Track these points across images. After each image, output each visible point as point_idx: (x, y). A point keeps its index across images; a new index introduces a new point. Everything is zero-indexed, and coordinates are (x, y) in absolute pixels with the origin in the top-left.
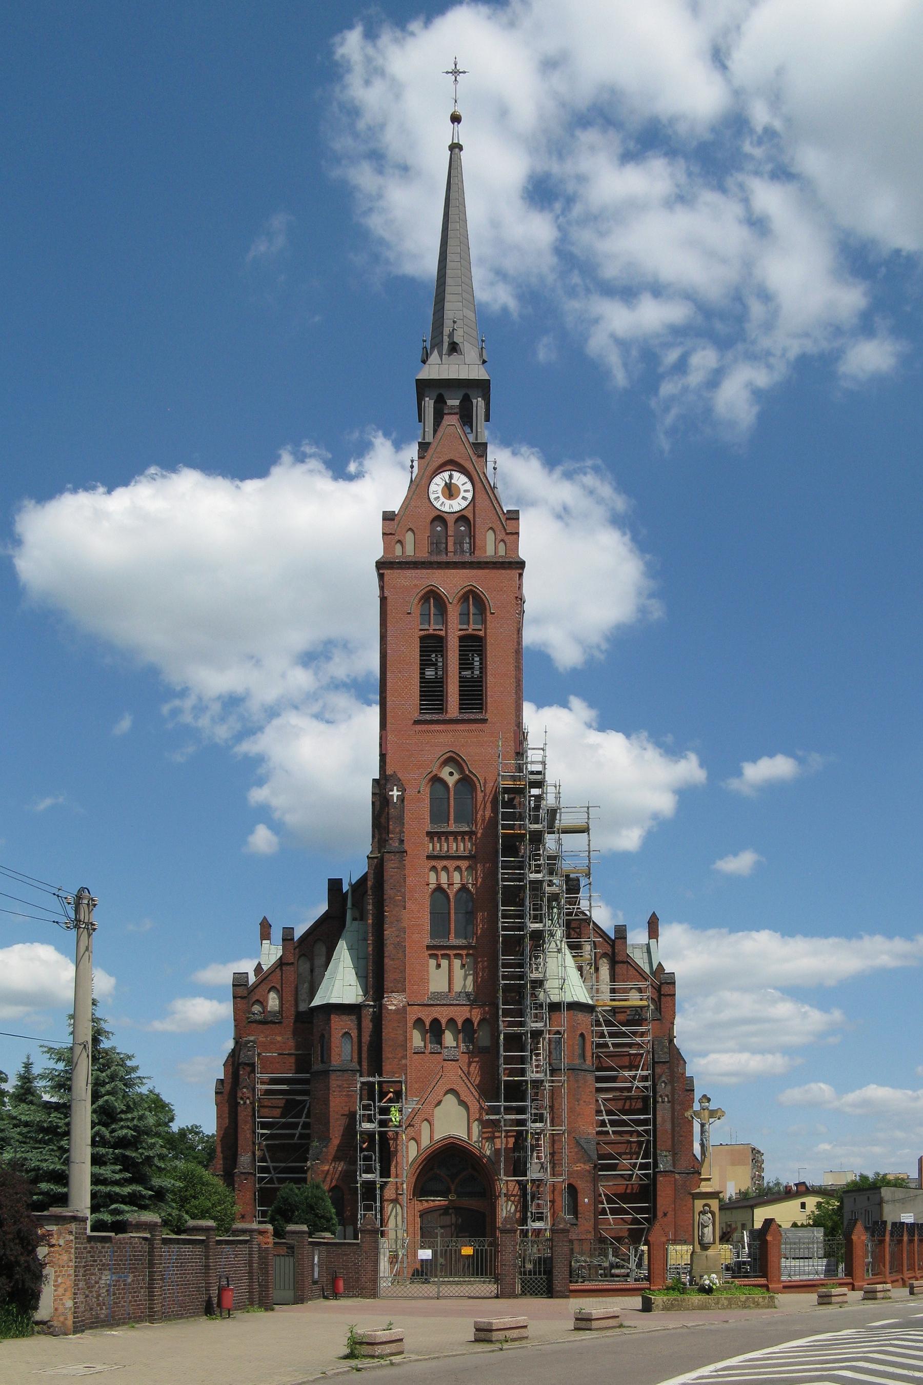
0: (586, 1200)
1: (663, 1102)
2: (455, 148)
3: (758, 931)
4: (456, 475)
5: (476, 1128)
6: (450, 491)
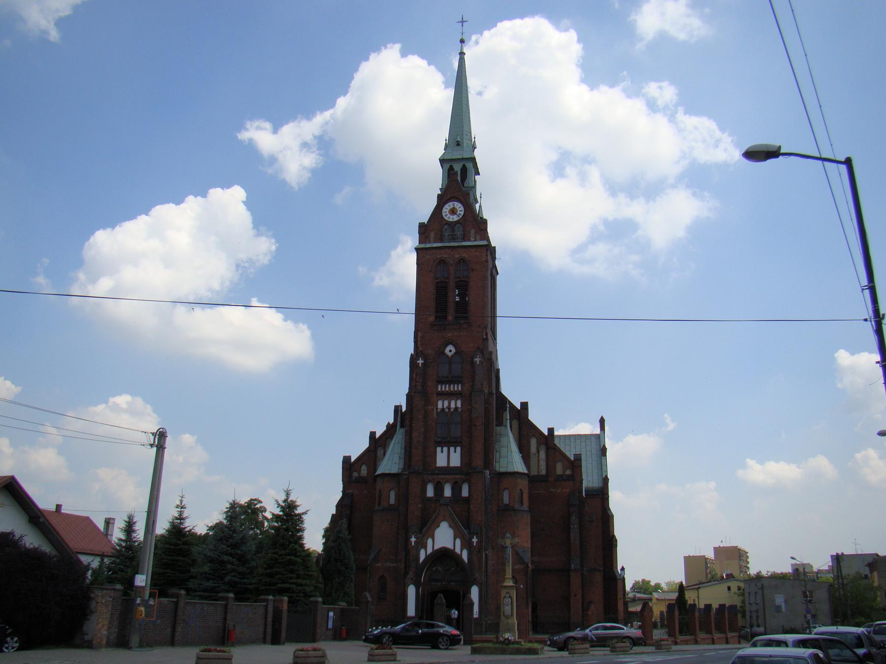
4: (456, 203)
5: (458, 542)
6: (453, 211)
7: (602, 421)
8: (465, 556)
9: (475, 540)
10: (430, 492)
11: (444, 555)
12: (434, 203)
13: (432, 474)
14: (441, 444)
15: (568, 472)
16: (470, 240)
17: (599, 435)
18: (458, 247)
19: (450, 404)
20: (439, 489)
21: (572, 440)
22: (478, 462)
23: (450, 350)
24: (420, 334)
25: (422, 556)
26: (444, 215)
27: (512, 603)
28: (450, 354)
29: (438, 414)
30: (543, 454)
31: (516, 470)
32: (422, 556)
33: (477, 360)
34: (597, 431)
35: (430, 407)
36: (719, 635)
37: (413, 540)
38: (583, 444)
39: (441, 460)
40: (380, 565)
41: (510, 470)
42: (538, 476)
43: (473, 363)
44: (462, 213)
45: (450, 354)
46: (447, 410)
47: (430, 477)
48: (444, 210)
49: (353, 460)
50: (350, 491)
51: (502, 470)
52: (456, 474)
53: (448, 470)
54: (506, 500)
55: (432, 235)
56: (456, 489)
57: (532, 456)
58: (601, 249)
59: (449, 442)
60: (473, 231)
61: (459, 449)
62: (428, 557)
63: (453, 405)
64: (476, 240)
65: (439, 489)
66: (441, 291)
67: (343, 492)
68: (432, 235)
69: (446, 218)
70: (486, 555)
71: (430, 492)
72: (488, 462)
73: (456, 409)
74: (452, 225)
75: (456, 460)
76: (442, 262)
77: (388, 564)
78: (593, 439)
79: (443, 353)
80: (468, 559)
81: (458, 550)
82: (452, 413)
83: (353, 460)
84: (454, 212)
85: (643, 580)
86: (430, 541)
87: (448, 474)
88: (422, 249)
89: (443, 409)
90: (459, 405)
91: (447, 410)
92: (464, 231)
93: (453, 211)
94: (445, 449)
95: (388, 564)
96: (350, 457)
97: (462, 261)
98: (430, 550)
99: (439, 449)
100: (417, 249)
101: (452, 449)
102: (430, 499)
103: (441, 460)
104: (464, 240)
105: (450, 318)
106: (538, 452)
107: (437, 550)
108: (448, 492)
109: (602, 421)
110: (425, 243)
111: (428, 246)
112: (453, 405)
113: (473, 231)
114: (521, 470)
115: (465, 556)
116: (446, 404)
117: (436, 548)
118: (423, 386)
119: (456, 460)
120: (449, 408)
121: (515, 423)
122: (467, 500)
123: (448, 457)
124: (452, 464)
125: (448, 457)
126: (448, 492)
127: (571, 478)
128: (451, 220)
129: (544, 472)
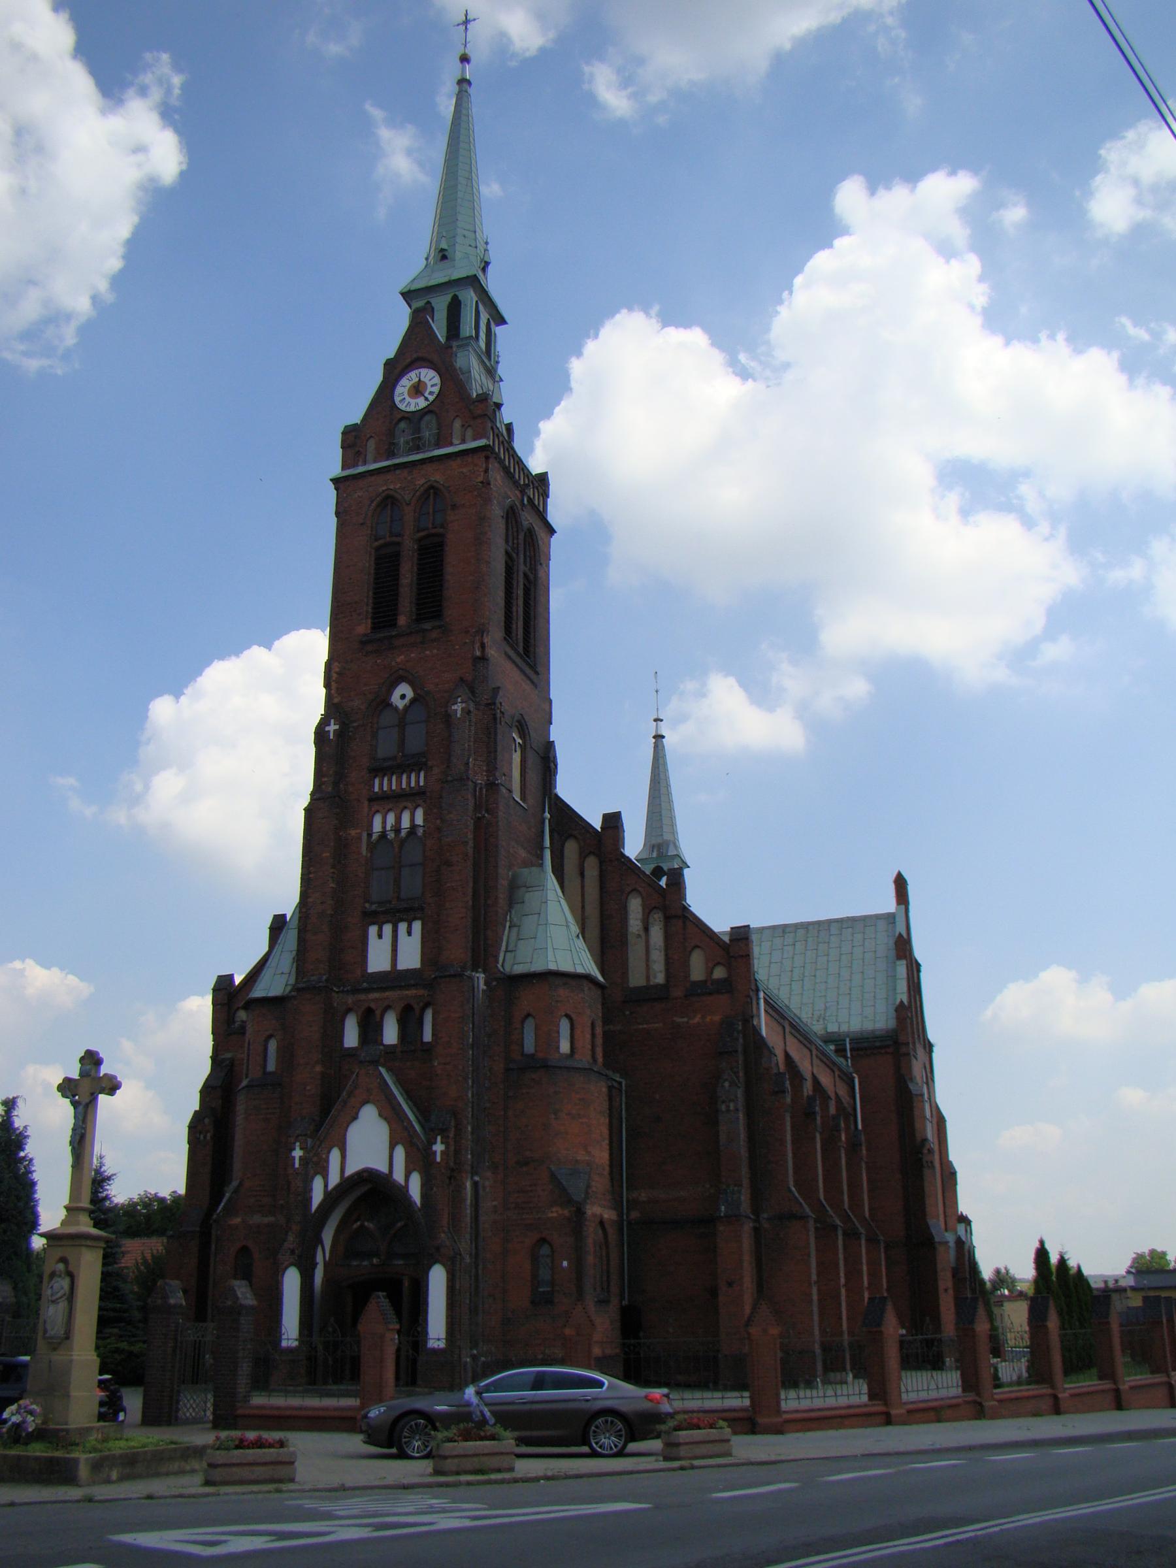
0: (565, 1263)
1: (728, 1110)
2: (463, 82)
3: (380, 1115)
4: (424, 371)
5: (400, 1153)
6: (417, 390)
7: (900, 884)
8: (415, 1190)
9: (439, 1147)
10: (351, 1037)
11: (370, 1189)
12: (378, 377)
13: (356, 991)
14: (376, 917)
15: (719, 973)
16: (451, 444)
17: (890, 918)
18: (423, 461)
19: (398, 820)
20: (370, 1028)
21: (834, 930)
22: (457, 951)
23: (401, 695)
24: (336, 667)
25: (317, 1197)
26: (397, 399)
27: (71, 1297)
28: (400, 704)
29: (372, 847)
30: (657, 934)
31: (552, 967)
32: (317, 1197)
33: (458, 708)
34: (888, 904)
35: (353, 832)
36: (1141, 1377)
37: (298, 1153)
38: (859, 937)
39: (378, 959)
40: (238, 1220)
41: (538, 966)
42: (647, 988)
43: (448, 718)
44: (436, 390)
45: (400, 704)
46: (391, 835)
47: (350, 1000)
48: (399, 390)
49: (238, 980)
50: (229, 1055)
51: (519, 969)
52: (408, 987)
53: (394, 979)
54: (529, 1046)
55: (371, 445)
56: (409, 1021)
57: (631, 939)
58: (1058, 651)
59: (395, 912)
60: (457, 424)
61: (417, 926)
62: (333, 1198)
63: (406, 823)
64: (463, 441)
65: (370, 1028)
66: (386, 564)
67: (215, 1059)
68: (371, 445)
69: (402, 407)
70: (475, 1184)
71: (351, 1037)
72: (483, 950)
73: (413, 827)
74: (408, 417)
75: (411, 956)
76: (389, 501)
77: (257, 1219)
78: (882, 925)
79: (386, 704)
80: (424, 1196)
81: (399, 1176)
82: (403, 842)
83: (238, 980)
84: (420, 389)
85: (1152, 1252)
86: (335, 1156)
87: (392, 988)
88: (346, 478)
89: (383, 835)
90: (419, 819)
91: (391, 835)
92: (439, 427)
93: (417, 390)
94: (388, 929)
95: (257, 1219)
96: (231, 977)
97: (432, 491)
98: (334, 1179)
99: (373, 930)
100: (336, 481)
101: (403, 927)
102: (351, 1053)
103: (378, 959)
104: (438, 446)
105: (402, 620)
106: (646, 929)
107: (352, 1176)
108: (391, 1034)
109: (900, 884)
110: (355, 465)
111: (361, 469)
112: (406, 823)
113: (457, 424)
114: (565, 964)
115: (415, 1190)
116: (391, 819)
117: (348, 1172)
118: (336, 784)
119: (411, 956)
120: (397, 829)
121: (592, 864)
122: (428, 1049)
123: (395, 949)
124: (402, 965)
125: (395, 949)
126: (391, 1034)
127: (726, 986)
128: (412, 408)
129: (660, 979)
